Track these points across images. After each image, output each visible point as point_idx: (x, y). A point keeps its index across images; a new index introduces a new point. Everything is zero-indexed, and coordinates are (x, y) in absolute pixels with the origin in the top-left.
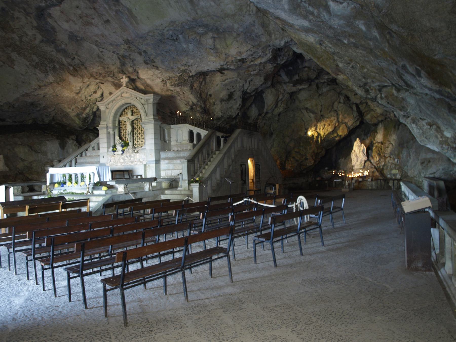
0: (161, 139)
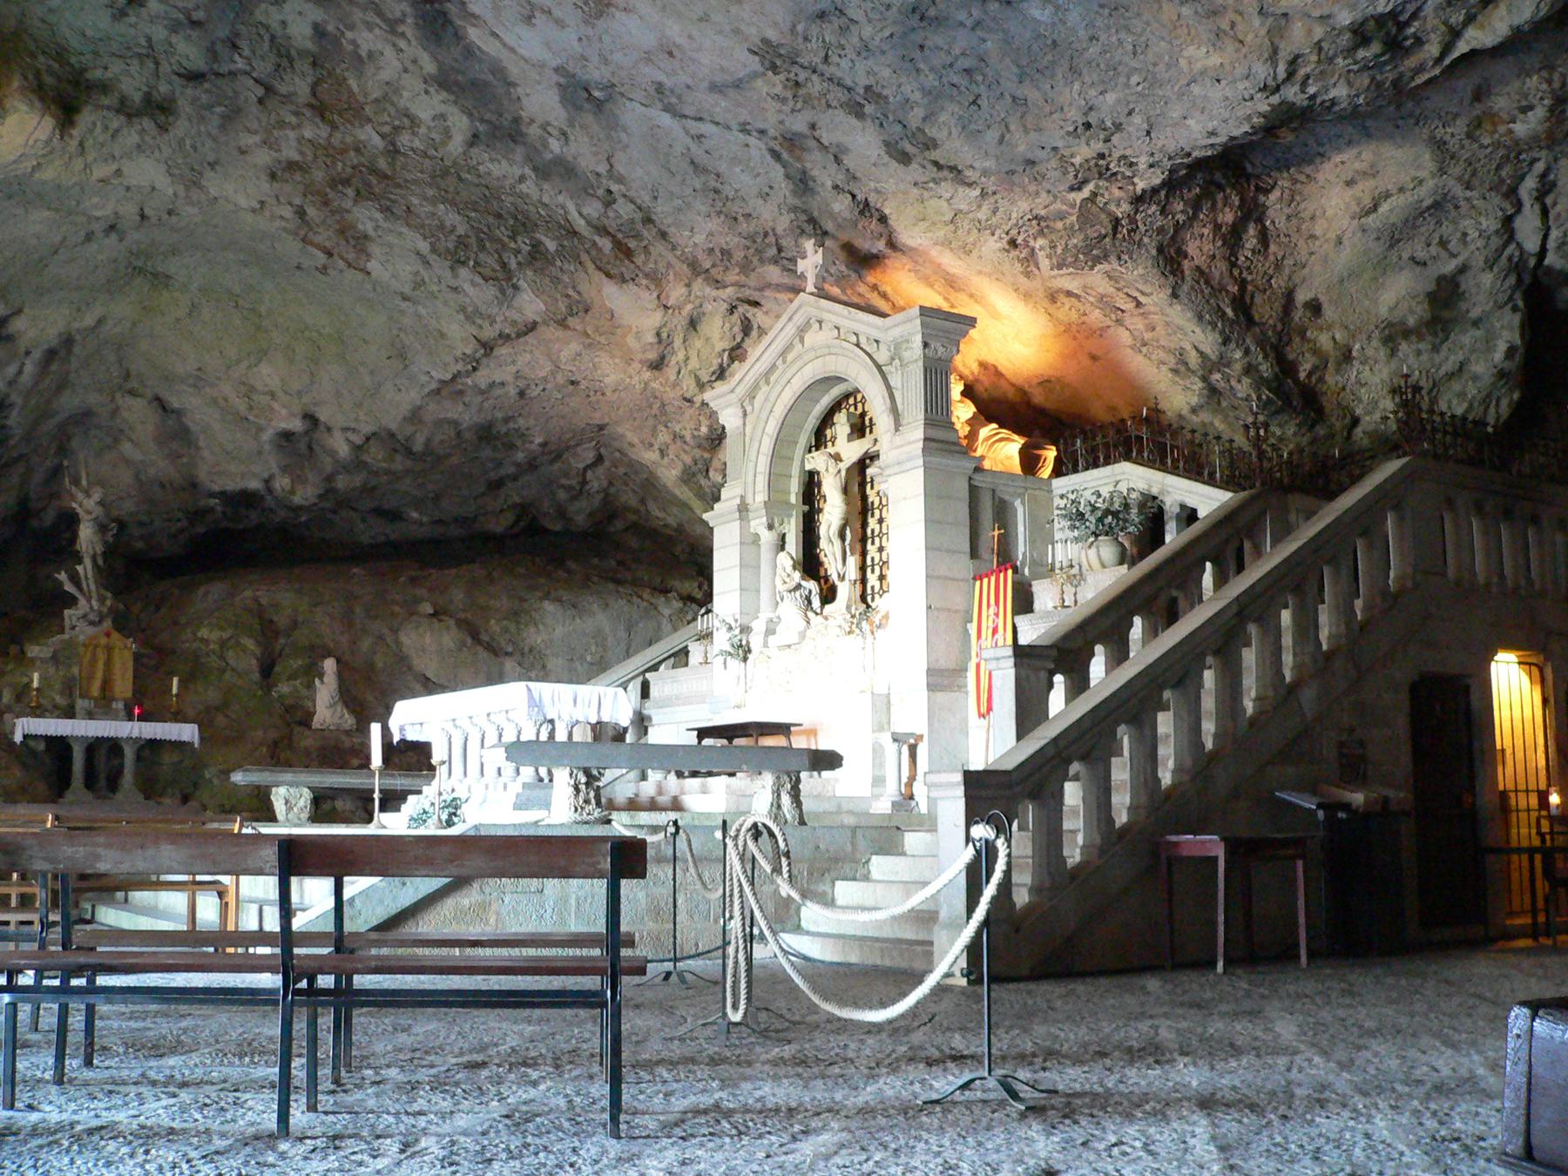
0: (974, 553)
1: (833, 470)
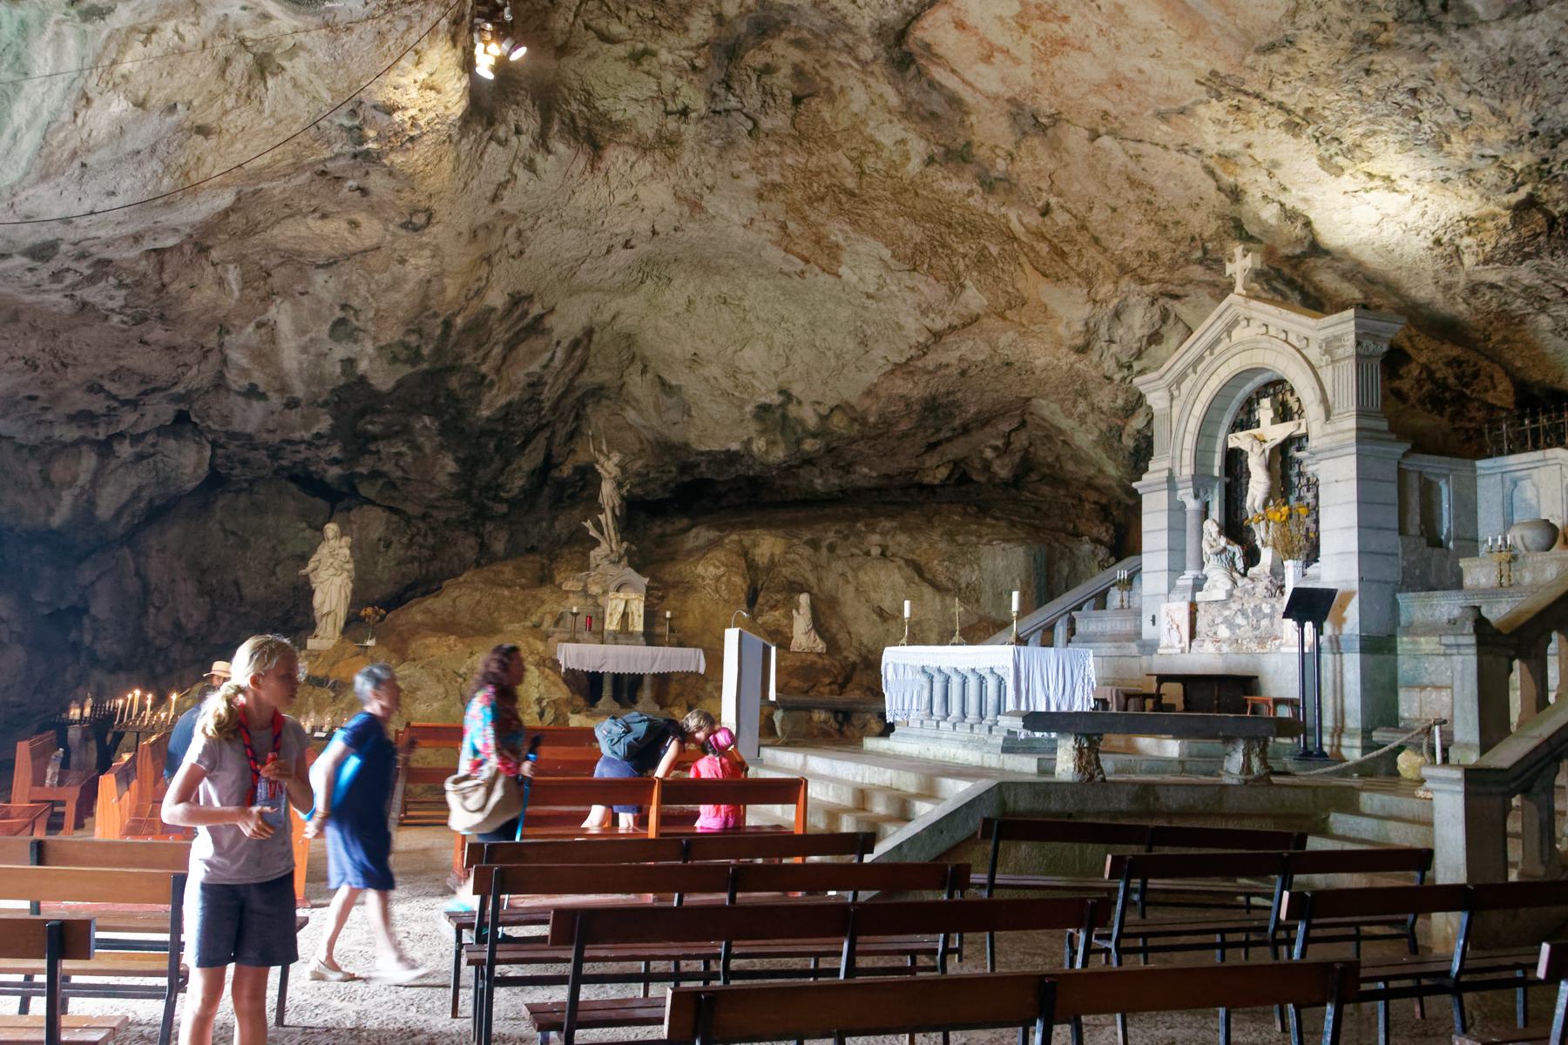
0: (1402, 531)
1: (1257, 449)
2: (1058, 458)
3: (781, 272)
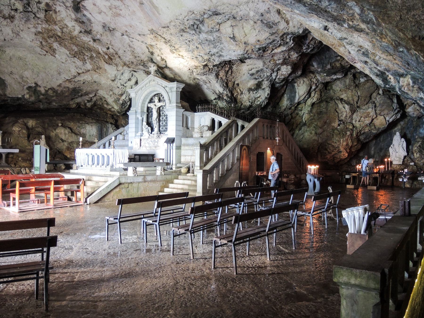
0: (183, 126)
2: (102, 104)
3: (39, 54)
